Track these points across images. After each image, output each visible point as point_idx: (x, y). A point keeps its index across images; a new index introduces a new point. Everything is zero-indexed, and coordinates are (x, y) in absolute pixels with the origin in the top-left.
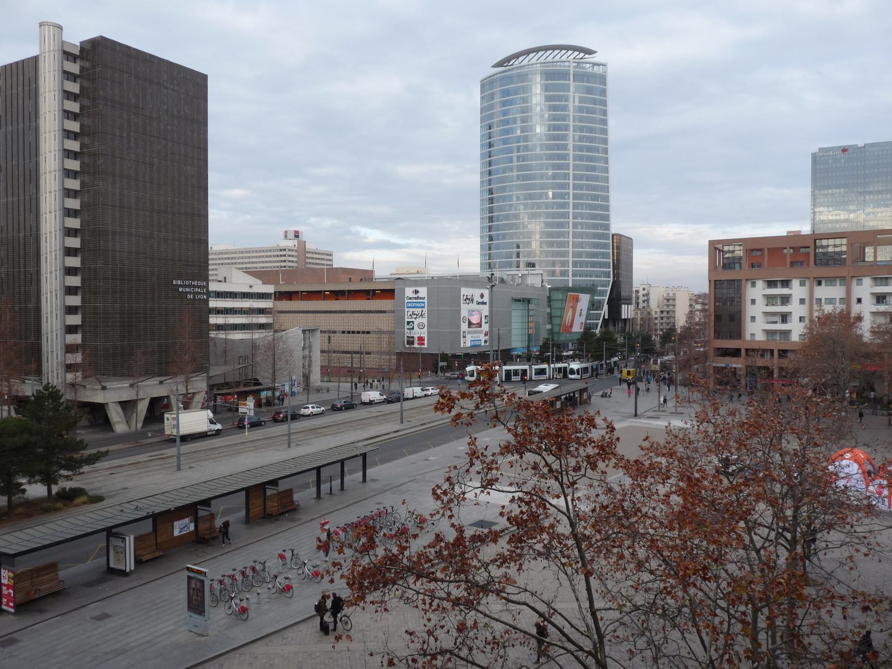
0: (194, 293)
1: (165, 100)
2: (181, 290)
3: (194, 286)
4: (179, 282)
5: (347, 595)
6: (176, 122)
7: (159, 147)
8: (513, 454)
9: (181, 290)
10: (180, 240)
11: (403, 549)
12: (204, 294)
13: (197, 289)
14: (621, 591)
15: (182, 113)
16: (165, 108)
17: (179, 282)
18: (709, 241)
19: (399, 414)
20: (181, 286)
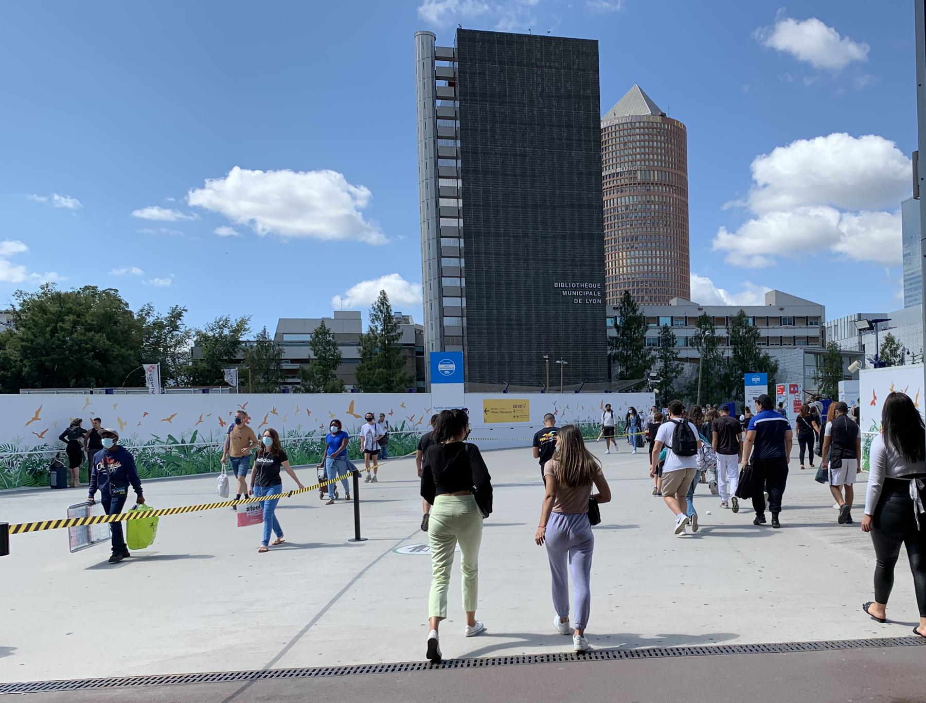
0: (583, 297)
1: (540, 81)
2: (564, 293)
3: (584, 289)
4: (562, 285)
5: (537, 530)
6: (555, 103)
7: (532, 134)
8: (732, 325)
9: (564, 293)
10: (564, 237)
11: (134, 360)
12: (598, 297)
13: (587, 293)
14: (835, 447)
15: (562, 90)
16: (540, 89)
17: (562, 285)
18: (239, 526)
19: (803, 380)
20: (565, 289)
